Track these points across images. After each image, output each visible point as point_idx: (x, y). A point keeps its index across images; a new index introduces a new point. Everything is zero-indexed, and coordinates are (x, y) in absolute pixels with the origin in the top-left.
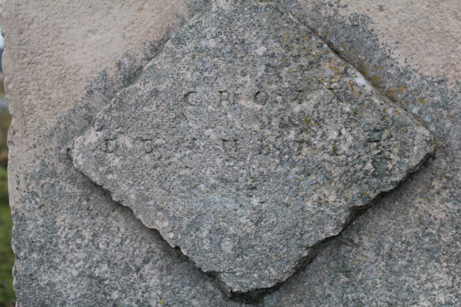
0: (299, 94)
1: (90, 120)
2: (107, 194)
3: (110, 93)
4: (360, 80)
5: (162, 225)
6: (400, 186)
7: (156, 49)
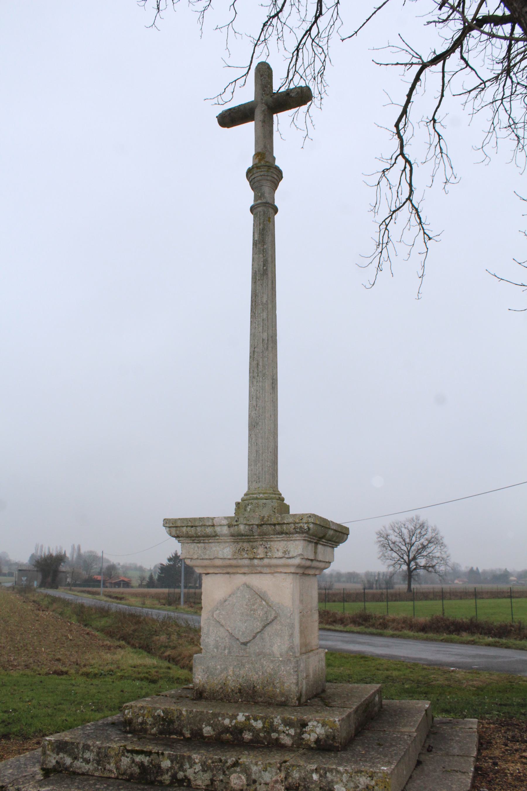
0: (254, 605)
1: (217, 609)
2: (220, 623)
3: (20, 625)
4: (264, 603)
5: (229, 629)
6: (271, 622)
7: (230, 596)
